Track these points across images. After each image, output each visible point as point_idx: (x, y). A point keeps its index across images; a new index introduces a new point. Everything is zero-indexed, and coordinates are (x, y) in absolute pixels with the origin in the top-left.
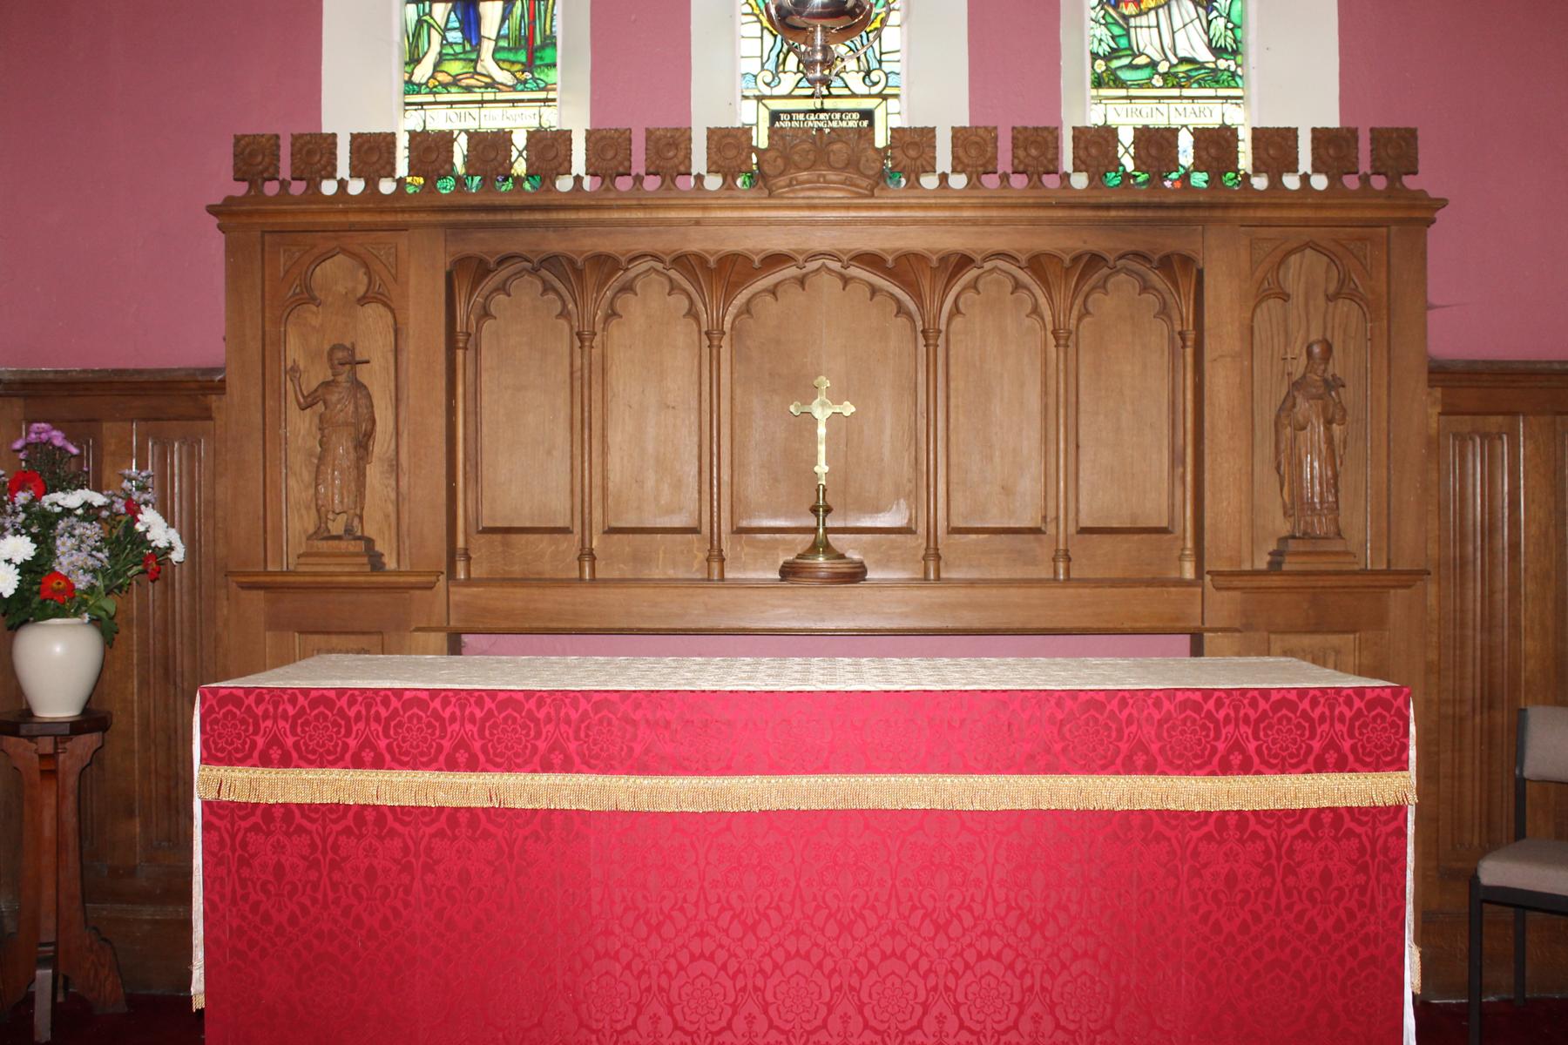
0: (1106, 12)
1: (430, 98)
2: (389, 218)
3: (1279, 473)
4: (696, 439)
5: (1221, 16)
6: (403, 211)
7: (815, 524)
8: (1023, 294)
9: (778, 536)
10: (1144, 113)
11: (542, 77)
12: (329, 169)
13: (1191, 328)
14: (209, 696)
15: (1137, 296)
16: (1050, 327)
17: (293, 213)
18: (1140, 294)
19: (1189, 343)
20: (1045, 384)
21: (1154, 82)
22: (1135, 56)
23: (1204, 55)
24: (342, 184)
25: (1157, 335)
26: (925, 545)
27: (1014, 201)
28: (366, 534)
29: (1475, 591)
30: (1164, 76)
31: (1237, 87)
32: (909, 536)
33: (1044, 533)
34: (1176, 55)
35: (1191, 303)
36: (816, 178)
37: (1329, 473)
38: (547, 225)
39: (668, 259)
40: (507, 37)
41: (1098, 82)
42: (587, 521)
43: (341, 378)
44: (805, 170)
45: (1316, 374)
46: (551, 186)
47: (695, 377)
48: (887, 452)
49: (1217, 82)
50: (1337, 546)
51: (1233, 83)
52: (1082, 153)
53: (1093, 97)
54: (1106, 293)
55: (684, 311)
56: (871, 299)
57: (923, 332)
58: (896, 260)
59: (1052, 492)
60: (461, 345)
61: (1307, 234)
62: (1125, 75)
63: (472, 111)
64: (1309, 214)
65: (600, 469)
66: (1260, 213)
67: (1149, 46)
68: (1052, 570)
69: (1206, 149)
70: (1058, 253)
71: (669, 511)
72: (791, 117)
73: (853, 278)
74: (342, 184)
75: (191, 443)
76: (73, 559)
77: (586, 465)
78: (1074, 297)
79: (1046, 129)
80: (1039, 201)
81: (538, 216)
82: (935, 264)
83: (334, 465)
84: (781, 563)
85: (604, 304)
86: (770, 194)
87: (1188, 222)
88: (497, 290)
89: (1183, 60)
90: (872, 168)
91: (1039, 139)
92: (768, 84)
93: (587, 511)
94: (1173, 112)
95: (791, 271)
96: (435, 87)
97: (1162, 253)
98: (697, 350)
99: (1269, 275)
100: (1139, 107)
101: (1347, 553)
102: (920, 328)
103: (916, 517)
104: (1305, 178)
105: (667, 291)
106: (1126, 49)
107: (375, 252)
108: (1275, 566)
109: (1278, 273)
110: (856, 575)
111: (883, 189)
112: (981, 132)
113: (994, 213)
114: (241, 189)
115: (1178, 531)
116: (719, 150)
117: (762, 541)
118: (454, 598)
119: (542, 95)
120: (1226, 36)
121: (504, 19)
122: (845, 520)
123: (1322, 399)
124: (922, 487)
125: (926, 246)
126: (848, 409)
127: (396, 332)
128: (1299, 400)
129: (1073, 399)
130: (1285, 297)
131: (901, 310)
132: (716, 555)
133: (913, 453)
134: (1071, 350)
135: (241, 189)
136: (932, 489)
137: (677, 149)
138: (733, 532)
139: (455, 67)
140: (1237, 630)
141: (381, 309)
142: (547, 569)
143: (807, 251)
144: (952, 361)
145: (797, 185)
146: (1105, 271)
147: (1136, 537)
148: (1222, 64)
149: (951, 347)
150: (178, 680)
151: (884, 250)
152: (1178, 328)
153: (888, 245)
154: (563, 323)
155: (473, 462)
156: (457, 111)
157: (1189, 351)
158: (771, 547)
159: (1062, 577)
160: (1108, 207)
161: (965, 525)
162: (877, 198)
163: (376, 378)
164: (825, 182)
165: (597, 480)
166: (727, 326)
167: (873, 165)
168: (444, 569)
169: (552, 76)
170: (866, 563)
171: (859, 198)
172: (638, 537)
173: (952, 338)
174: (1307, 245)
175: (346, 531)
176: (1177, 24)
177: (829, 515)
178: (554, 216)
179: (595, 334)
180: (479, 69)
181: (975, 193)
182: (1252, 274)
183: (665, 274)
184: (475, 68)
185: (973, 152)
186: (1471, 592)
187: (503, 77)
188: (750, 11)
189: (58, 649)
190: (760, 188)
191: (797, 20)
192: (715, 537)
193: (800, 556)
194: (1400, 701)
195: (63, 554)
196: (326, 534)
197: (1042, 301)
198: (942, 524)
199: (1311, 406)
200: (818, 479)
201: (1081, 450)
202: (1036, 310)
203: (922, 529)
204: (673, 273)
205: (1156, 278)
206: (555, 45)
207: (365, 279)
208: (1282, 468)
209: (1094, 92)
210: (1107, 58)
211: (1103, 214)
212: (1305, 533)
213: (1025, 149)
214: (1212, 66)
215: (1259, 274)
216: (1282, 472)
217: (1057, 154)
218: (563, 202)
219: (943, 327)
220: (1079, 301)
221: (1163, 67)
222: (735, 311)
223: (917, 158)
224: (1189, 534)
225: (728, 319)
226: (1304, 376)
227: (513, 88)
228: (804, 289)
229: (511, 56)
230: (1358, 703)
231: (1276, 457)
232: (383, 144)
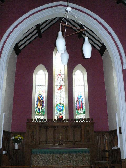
23: (83, 113)
41: (76, 114)
114: (27, 122)
135: (27, 122)
187: (41, 114)
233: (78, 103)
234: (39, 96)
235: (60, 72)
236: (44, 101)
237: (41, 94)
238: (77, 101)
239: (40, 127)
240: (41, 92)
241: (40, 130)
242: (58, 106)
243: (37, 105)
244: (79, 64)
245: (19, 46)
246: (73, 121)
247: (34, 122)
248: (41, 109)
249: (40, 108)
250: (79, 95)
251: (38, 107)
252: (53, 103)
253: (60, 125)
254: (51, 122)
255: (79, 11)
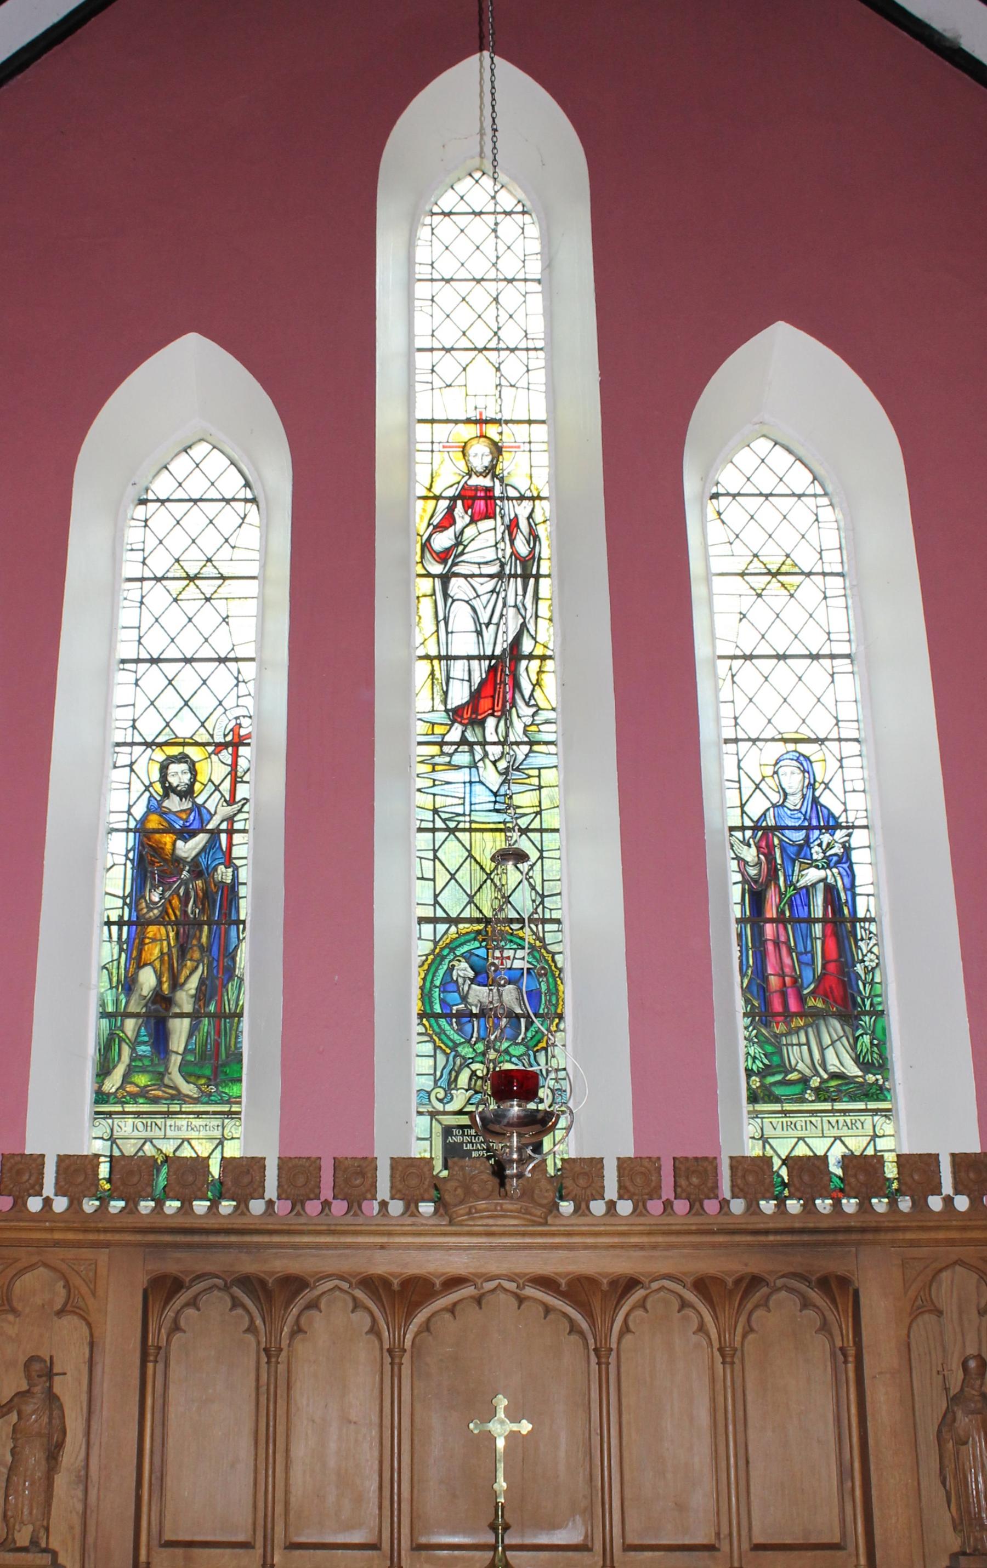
0: (759, 1031)
1: (118, 1108)
2: (92, 1237)
3: (944, 1485)
4: (376, 1454)
5: (866, 1034)
6: (106, 1231)
7: (493, 1541)
8: (689, 1312)
11: (227, 1090)
12: (37, 1188)
13: (851, 1343)
15: (798, 1313)
16: (716, 1345)
18: (801, 1311)
19: (851, 1359)
20: (713, 1400)
21: (807, 1096)
22: (787, 1073)
23: (853, 1070)
24: (48, 1202)
25: (819, 1347)
26: (601, 1563)
27: (678, 1227)
28: (51, 1546)
30: (817, 1090)
32: (586, 1553)
33: (718, 1550)
34: (825, 1070)
35: (850, 1320)
36: (493, 1208)
38: (240, 1246)
39: (354, 1281)
40: (192, 1051)
42: (269, 1536)
43: (37, 1389)
44: (483, 1199)
45: (973, 1389)
46: (245, 1210)
47: (376, 1392)
55: (367, 1328)
56: (545, 1318)
57: (594, 1350)
58: (569, 1284)
59: (724, 1508)
60: (152, 1358)
61: (956, 1252)
62: (778, 1091)
65: (282, 1484)
66: (909, 1236)
69: (855, 1176)
70: (719, 1275)
71: (349, 1527)
72: (463, 1132)
73: (527, 1298)
74: (48, 1202)
77: (270, 1479)
78: (739, 1313)
79: (706, 1158)
80: (701, 1227)
81: (233, 1239)
82: (605, 1287)
83: (25, 1476)
85: (291, 1319)
86: (450, 1221)
88: (187, 1305)
89: (834, 1076)
90: (546, 1198)
91: (700, 1168)
92: (440, 1100)
93: (269, 1526)
94: (826, 1125)
95: (468, 1291)
96: (124, 1097)
97: (818, 1275)
99: (922, 1293)
100: (794, 1120)
102: (592, 1346)
103: (592, 1534)
104: (948, 1201)
105: (351, 1308)
106: (778, 1066)
107: (75, 1267)
109: (930, 1290)
111: (555, 1217)
112: (646, 1163)
113: (660, 1239)
115: (851, 1547)
116: (403, 1180)
117: (440, 1558)
119: (226, 1108)
121: (190, 1036)
122: (523, 1536)
123: (980, 1413)
125: (598, 1270)
126: (525, 1427)
127: (92, 1345)
128: (959, 1414)
129: (741, 1413)
131: (574, 1328)
133: (588, 1469)
134: (738, 1367)
136: (607, 1506)
137: (363, 1177)
138: (413, 1549)
139: (142, 1080)
141: (75, 1320)
143: (486, 1274)
145: (476, 1213)
146: (765, 1290)
147: (809, 1554)
148: (871, 1078)
149: (622, 1365)
151: (556, 1274)
154: (250, 1338)
155: (159, 1474)
156: (144, 1121)
157: (851, 1366)
160: (767, 1232)
161: (640, 1542)
162: (551, 1225)
164: (502, 1210)
165: (280, 1495)
166: (408, 1344)
167: (546, 1194)
169: (234, 1090)
171: (533, 1225)
172: (319, 1552)
174: (955, 1263)
175: (32, 1542)
176: (827, 1040)
177: (508, 1532)
178: (247, 1239)
179: (281, 1350)
181: (642, 1220)
182: (906, 1293)
183: (349, 1293)
185: (639, 1181)
187: (188, 1089)
190: (441, 1216)
191: (497, 1128)
196: (12, 1546)
197: (708, 1318)
198: (617, 1542)
199: (971, 1421)
201: (751, 1465)
202: (702, 1328)
203: (598, 1547)
204: (359, 1294)
205: (815, 1296)
207: (63, 1292)
208: (948, 1483)
209: (751, 1108)
210: (762, 1074)
211: (762, 1238)
212: (975, 1549)
214: (861, 1080)
215: (912, 1293)
216: (948, 1487)
218: (257, 1227)
219: (614, 1346)
220: (743, 1319)
221: (815, 1082)
222: (416, 1329)
223: (585, 1188)
224: (862, 1550)
225: (409, 1337)
226: (962, 1389)
227: (196, 1101)
228: (481, 1308)
231: (941, 1472)
232: (89, 1166)
233: (780, 920)
234: (154, 822)
236: (231, 892)
237: (188, 793)
238: (756, 898)
240: (194, 753)
242: (463, 970)
244: (780, 323)
246: (713, 1191)
248: (195, 1016)
250: (794, 801)
251: (147, 979)
252: (294, 485)
253: (493, 1267)
254: (339, 1207)
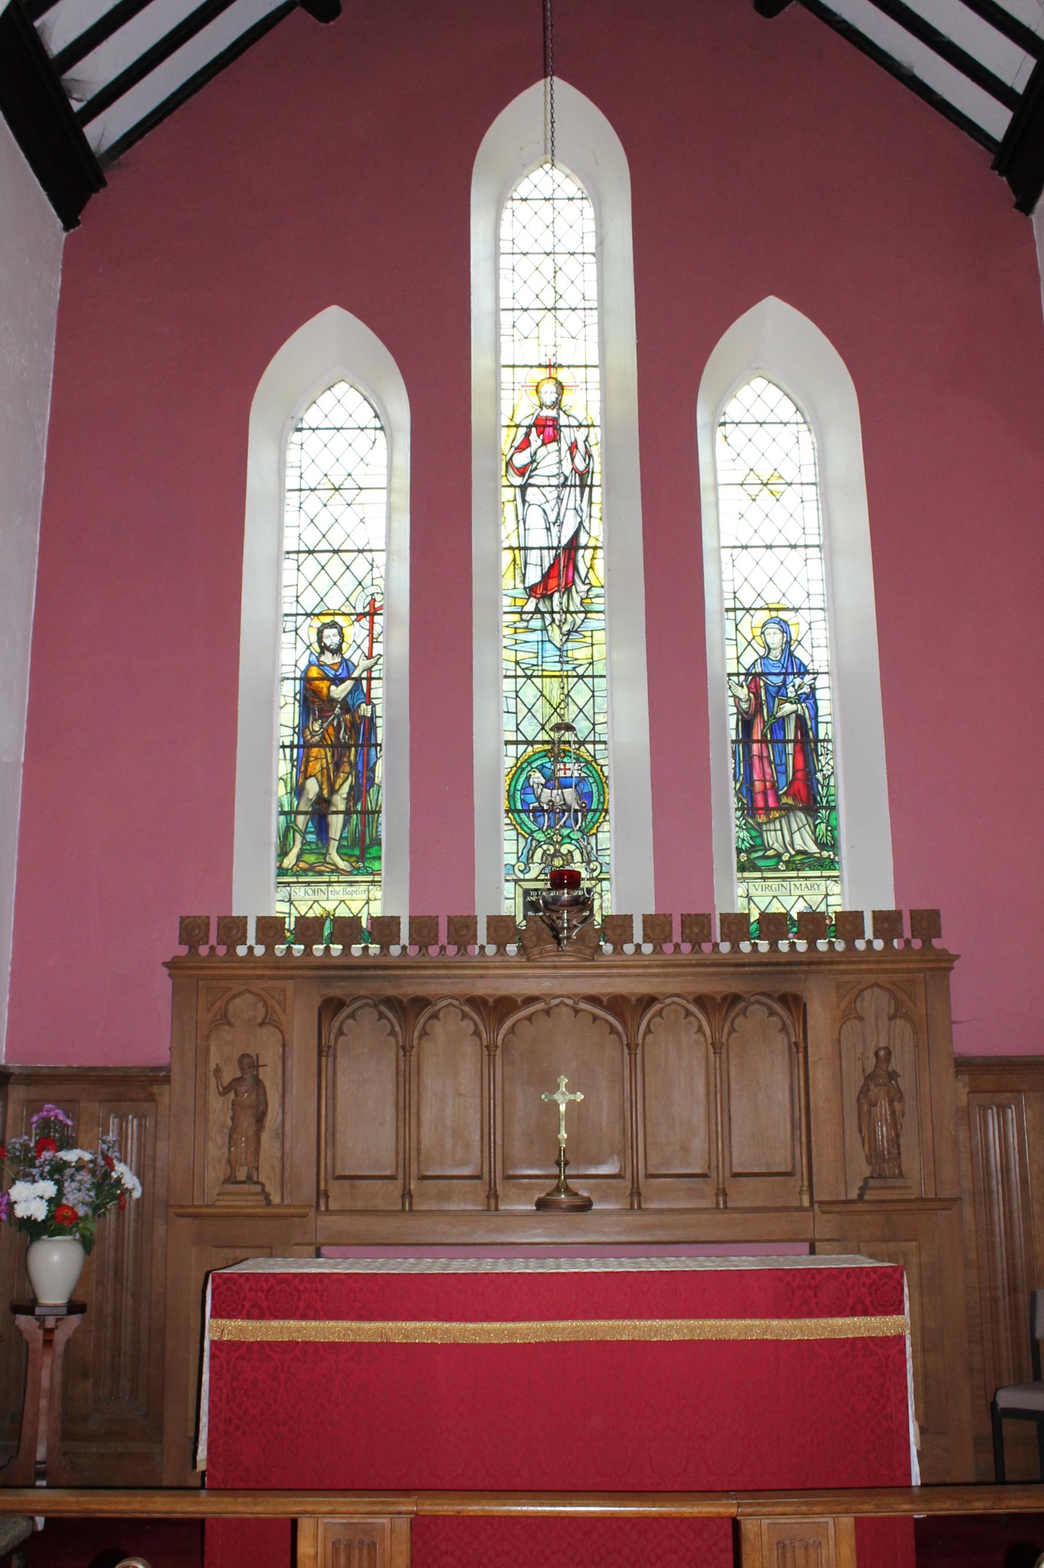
0: (747, 821)
1: (295, 880)
2: (282, 972)
4: (479, 1116)
5: (823, 822)
8: (691, 1018)
9: (534, 1181)
10: (774, 889)
11: (370, 866)
14: (217, 1278)
16: (710, 1041)
17: (220, 968)
21: (780, 867)
22: (766, 850)
23: (813, 848)
24: (251, 949)
25: (780, 1042)
26: (630, 1186)
29: (999, 1211)
30: (787, 863)
31: (835, 869)
34: (793, 848)
37: (893, 1135)
39: (462, 1000)
40: (346, 838)
41: (742, 868)
43: (247, 1076)
47: (479, 1075)
48: (604, 1124)
49: (822, 866)
50: (900, 1182)
51: (832, 867)
52: (726, 930)
53: (738, 879)
54: (746, 1017)
55: (471, 1032)
60: (325, 1054)
61: (873, 978)
62: (760, 863)
63: (323, 888)
64: (873, 966)
66: (841, 967)
67: (776, 843)
68: (715, 1202)
69: (805, 926)
73: (581, 1010)
74: (251, 949)
75: (141, 1117)
76: (76, 1196)
77: (407, 1134)
78: (725, 1020)
79: (703, 915)
81: (379, 972)
82: (634, 1002)
84: (536, 1199)
85: (419, 1026)
87: (794, 973)
88: (348, 1017)
89: (799, 852)
92: (522, 871)
94: (793, 887)
95: (541, 1006)
96: (298, 871)
98: (479, 1058)
100: (770, 884)
101: (906, 1187)
102: (625, 1043)
104: (869, 943)
106: (760, 845)
108: (861, 1197)
110: (585, 1206)
113: (671, 970)
117: (522, 1184)
118: (320, 1223)
119: (370, 878)
120: (827, 836)
124: (627, 1149)
126: (580, 1097)
127: (284, 1046)
128: (872, 1087)
129: (725, 1087)
130: (861, 1019)
131: (613, 1030)
132: (493, 1195)
134: (724, 1056)
139: (312, 859)
140: (838, 1240)
141: (272, 1029)
142: (380, 1204)
144: (646, 1064)
148: (825, 854)
150: (124, 1281)
152: (793, 1039)
153: (603, 991)
154: (392, 1040)
157: (801, 1055)
158: (528, 1188)
159: (722, 1206)
160: (744, 965)
163: (269, 1076)
165: (414, 1144)
166: (499, 1042)
168: (315, 1205)
170: (592, 1198)
173: (646, 1048)
174: (873, 985)
176: (795, 827)
180: (328, 859)
182: (838, 1006)
184: (325, 859)
186: (996, 1212)
187: (342, 864)
188: (509, 822)
189: (56, 1258)
192: (493, 1182)
193: (548, 1194)
194: (897, 1275)
195: (69, 1192)
197: (705, 1023)
198: (642, 1172)
200: (560, 1144)
202: (700, 1030)
203: (628, 1175)
205: (777, 1007)
206: (380, 844)
207: (263, 1010)
209: (740, 875)
210: (748, 851)
211: (740, 969)
213: (690, 928)
214: (818, 855)
215: (843, 1005)
217: (710, 930)
219: (640, 1041)
221: (786, 857)
225: (500, 1037)
227: (350, 873)
229: (349, 852)
230: (873, 1276)
233: (763, 741)
234: (314, 672)
235: (557, 404)
236: (370, 723)
238: (746, 724)
239: (331, 1007)
240: (340, 620)
241: (323, 1051)
242: (537, 778)
243: (302, 769)
245: (76, 106)
246: (708, 937)
247: (260, 950)
248: (347, 813)
249: (328, 802)
251: (312, 787)
254: (452, 950)
255: (195, 1397)
